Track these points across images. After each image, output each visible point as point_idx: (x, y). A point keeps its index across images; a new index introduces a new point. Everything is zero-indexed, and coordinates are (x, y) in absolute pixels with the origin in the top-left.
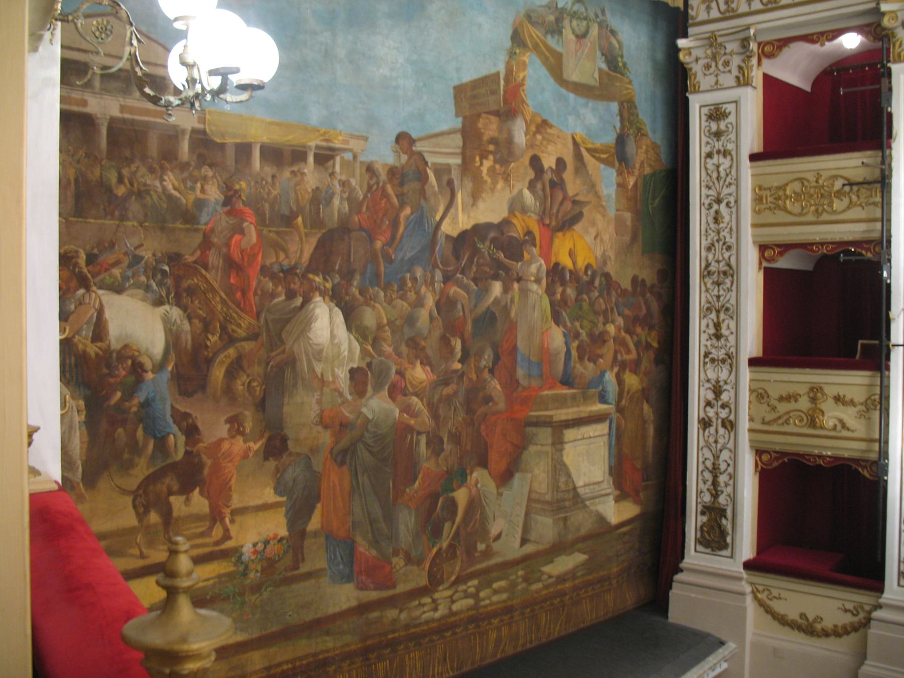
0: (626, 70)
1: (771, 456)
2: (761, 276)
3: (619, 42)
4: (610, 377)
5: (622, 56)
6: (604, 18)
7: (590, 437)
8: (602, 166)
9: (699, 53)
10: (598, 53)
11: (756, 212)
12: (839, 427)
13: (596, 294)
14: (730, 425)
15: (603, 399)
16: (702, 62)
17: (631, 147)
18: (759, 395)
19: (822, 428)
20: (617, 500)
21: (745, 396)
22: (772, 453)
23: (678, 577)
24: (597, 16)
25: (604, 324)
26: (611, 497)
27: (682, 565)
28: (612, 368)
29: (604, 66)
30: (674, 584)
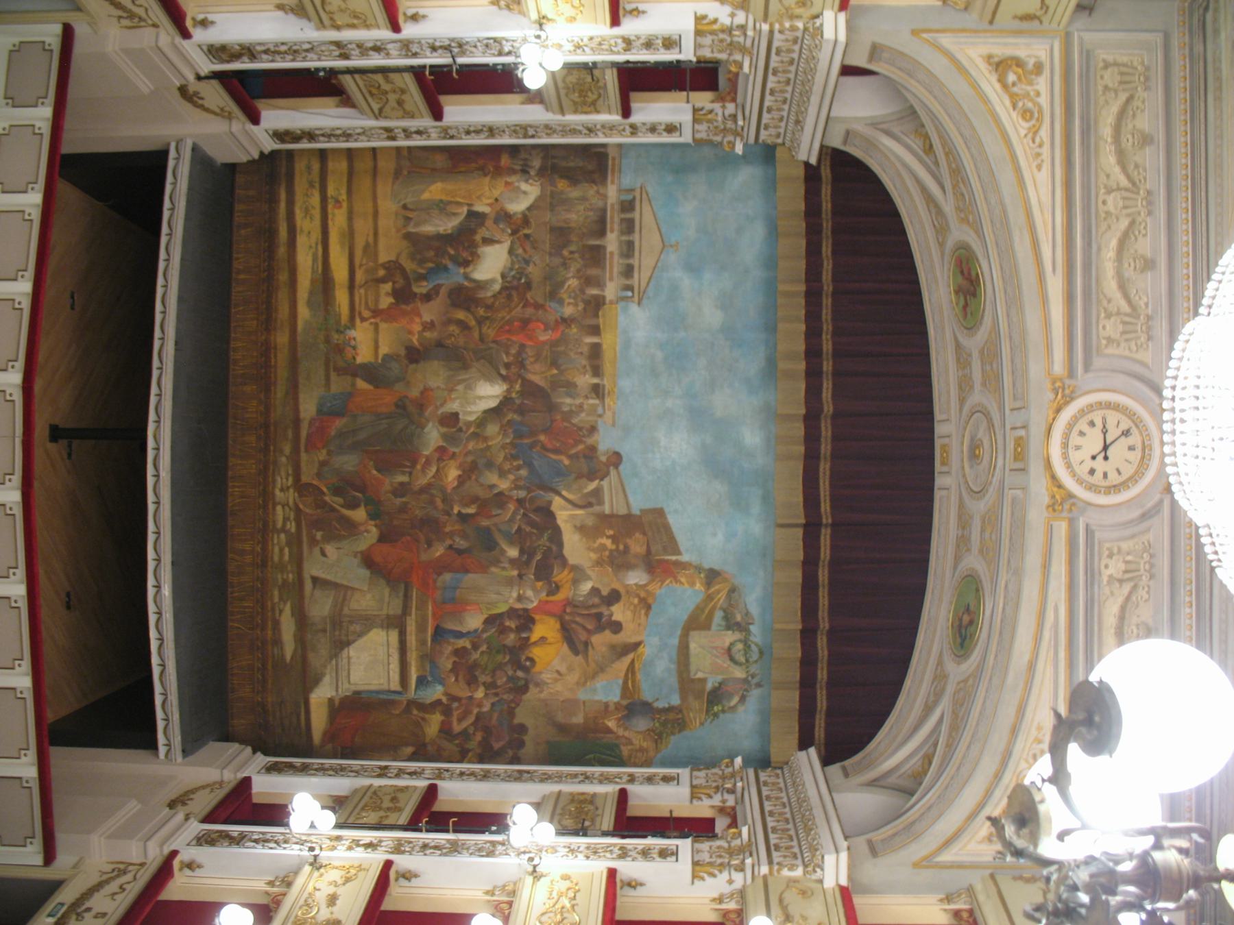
4: (436, 692)
5: (723, 711)
7: (389, 664)
8: (621, 682)
10: (719, 678)
11: (571, 794)
13: (510, 673)
15: (421, 681)
16: (720, 773)
17: (642, 724)
20: (331, 700)
23: (249, 749)
24: (753, 676)
25: (484, 684)
26: (334, 693)
29: (709, 686)
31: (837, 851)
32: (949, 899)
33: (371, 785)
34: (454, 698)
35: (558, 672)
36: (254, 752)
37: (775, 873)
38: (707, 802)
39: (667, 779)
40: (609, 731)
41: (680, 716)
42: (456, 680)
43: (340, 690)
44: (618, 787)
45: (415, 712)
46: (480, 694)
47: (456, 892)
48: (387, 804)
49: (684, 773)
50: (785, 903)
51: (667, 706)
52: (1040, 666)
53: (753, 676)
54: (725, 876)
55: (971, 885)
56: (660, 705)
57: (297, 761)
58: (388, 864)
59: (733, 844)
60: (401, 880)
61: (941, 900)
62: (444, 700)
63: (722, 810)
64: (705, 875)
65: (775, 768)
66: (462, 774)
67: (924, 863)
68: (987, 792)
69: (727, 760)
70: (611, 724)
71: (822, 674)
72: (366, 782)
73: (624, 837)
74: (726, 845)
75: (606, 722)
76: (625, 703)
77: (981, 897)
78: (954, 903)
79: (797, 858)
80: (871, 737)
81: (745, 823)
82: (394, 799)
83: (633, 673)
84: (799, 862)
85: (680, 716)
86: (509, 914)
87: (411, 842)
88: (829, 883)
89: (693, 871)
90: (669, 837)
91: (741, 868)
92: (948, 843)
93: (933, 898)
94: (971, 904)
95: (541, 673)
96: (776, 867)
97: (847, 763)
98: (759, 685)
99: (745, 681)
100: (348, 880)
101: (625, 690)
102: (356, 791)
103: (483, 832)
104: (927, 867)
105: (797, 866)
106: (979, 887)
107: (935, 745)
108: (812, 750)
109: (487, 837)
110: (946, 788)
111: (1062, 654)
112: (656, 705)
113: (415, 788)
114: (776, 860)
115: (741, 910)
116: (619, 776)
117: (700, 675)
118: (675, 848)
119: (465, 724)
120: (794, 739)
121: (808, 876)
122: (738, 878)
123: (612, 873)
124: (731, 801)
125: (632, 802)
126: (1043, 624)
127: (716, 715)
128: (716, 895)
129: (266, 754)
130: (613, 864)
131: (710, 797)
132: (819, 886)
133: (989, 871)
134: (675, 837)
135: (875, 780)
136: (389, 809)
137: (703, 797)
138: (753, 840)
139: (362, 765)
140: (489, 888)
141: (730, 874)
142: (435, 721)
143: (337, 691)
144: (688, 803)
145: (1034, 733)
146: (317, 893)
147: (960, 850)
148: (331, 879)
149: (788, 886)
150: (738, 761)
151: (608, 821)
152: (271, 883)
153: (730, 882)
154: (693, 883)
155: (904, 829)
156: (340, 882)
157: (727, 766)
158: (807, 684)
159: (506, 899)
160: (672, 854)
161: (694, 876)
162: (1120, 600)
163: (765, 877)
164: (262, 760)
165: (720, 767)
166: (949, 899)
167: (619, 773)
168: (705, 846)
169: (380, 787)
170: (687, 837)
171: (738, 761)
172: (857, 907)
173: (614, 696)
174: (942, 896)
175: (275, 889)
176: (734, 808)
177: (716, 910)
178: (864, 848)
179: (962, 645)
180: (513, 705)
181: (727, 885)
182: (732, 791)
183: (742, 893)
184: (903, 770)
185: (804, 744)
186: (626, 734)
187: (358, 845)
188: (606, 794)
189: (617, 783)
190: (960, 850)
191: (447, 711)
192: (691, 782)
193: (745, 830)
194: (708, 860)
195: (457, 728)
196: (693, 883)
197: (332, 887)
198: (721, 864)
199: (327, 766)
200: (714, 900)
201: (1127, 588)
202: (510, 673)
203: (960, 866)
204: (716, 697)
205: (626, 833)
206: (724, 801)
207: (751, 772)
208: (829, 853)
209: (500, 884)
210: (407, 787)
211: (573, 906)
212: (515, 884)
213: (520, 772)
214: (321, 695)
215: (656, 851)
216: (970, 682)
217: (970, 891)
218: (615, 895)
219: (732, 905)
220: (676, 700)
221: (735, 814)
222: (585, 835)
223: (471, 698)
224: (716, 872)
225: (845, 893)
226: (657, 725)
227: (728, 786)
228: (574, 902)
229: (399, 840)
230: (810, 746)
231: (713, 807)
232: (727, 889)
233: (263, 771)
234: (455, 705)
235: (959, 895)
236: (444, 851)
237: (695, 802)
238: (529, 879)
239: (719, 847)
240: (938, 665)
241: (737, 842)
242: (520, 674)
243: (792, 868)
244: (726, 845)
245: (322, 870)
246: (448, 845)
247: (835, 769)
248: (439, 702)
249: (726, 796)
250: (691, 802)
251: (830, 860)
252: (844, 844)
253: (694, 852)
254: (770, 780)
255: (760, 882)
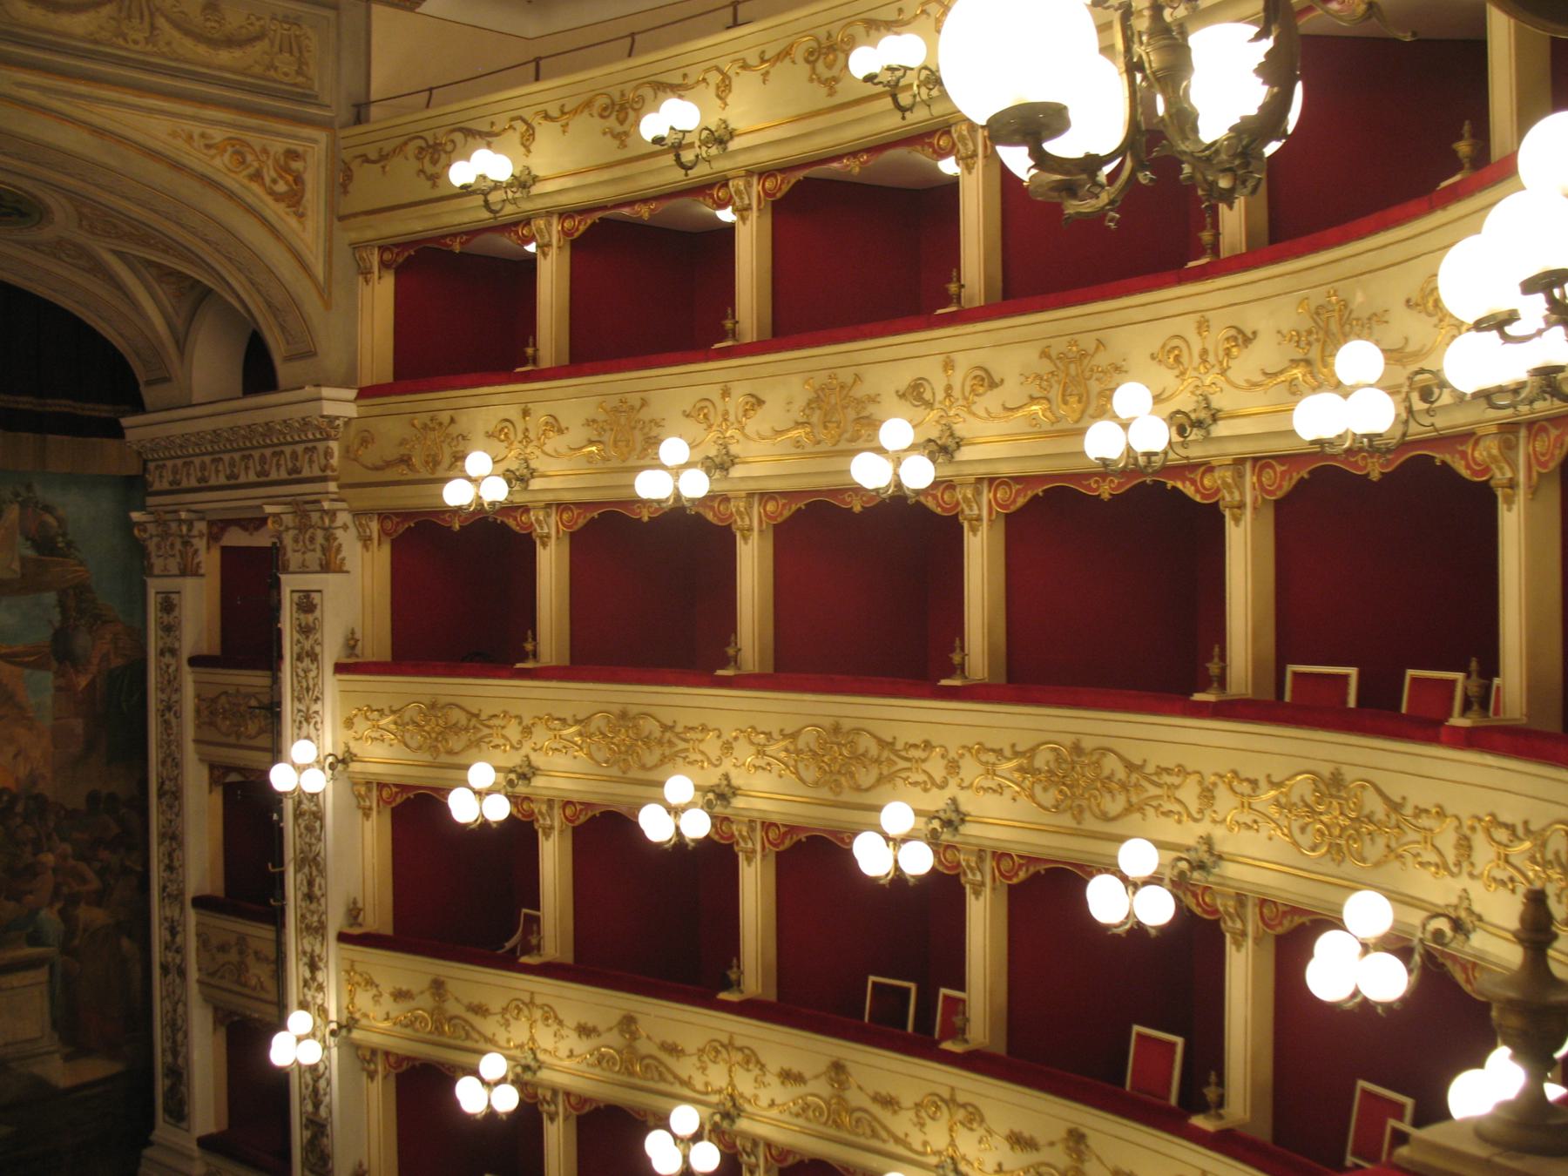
0: (72, 550)
1: (1014, 863)
2: (217, 799)
3: (58, 519)
4: (49, 917)
5: (64, 535)
6: (31, 495)
7: (13, 988)
8: (27, 672)
9: (151, 528)
10: (19, 539)
11: (198, 727)
12: (258, 988)
13: (19, 821)
14: (182, 972)
15: (35, 939)
16: (155, 540)
17: (82, 641)
18: (203, 940)
19: (245, 985)
20: (67, 1058)
21: (192, 944)
22: (1015, 858)
23: (147, 1152)
24: (17, 495)
25: (35, 855)
26: (57, 1056)
27: (153, 1137)
28: (51, 905)
29: (31, 553)
30: (143, 1161)
31: (320, 399)
32: (365, 273)
33: (199, 982)
34: (56, 893)
35: (15, 756)
36: (149, 1144)
37: (335, 473)
38: (203, 556)
39: (168, 606)
40: (91, 684)
41: (71, 592)
42: (31, 892)
43: (52, 1048)
44: (186, 668)
45: (76, 942)
46: (49, 859)
47: (368, 852)
48: (233, 956)
49: (154, 586)
50: (380, 463)
51: (58, 609)
52: (97, 121)
53: (17, 495)
54: (339, 533)
55: (350, 245)
56: (56, 617)
57: (161, 1085)
58: (343, 938)
59: (154, 533)
60: (360, 919)
61: (367, 282)
62: (58, 906)
63: (213, 537)
64: (339, 557)
65: (145, 469)
66: (170, 868)
67: (326, 297)
68: (248, 211)
69: (136, 532)
70: (83, 682)
71: (25, 403)
72: (194, 989)
73: (280, 657)
74: (292, 533)
75: (80, 688)
76: (55, 665)
77: (370, 234)
78: (371, 267)
79: (315, 448)
80: (106, 344)
81: (260, 507)
82: (223, 948)
83: (15, 655)
84: (321, 446)
85: (71, 592)
86: (396, 786)
87: (303, 916)
88: (351, 410)
89: (335, 572)
90: (279, 602)
91: (333, 514)
92: (305, 267)
93: (364, 291)
94: (373, 246)
95: (17, 779)
96: (329, 473)
97: (141, 378)
98: (29, 487)
99: (23, 505)
100: (370, 983)
101: (38, 665)
102: (207, 999)
103: (281, 830)
104: (330, 293)
105: (328, 447)
106: (353, 236)
107: (149, 264)
108: (125, 422)
109: (289, 824)
110: (230, 260)
111: (82, 88)
112: (57, 625)
113: (198, 924)
114: (317, 472)
115: (379, 515)
116: (163, 670)
117: (16, 566)
118: (296, 596)
119: (90, 875)
120: (110, 445)
121: (340, 435)
122: (343, 517)
123: (340, 668)
124: (201, 526)
125: (205, 650)
126: (42, 107)
127: (69, 545)
128: (359, 545)
129: (150, 1125)
130: (328, 668)
131: (196, 551)
132: (354, 422)
133: (335, 221)
134: (279, 593)
135: (177, 342)
136: (241, 952)
137: (196, 561)
138: (289, 499)
139: (162, 999)
140: (360, 813)
141: (195, 537)
142: (91, 916)
143: (48, 1053)
144: (203, 581)
145: (179, 143)
146: (393, 1015)
147: (311, 252)
148: (371, 1003)
149: (355, 460)
150: (136, 516)
151: (254, 680)
152: (372, 1076)
153: (345, 527)
154: (347, 572)
155: (275, 317)
156: (374, 991)
157: (145, 530)
158: (39, 424)
159: (375, 793)
160: (307, 597)
161: (341, 571)
162: (177, 35)
163: (340, 487)
164: (163, 1130)
165: (144, 540)
166: (365, 273)
167: (159, 668)
168: (294, 559)
169: (200, 969)
170: (278, 581)
171: (136, 516)
172: (375, 382)
173: (47, 679)
174: (361, 279)
175: (380, 1068)
176: (211, 523)
177: (379, 544)
178: (298, 367)
179: (22, 214)
180: (63, 812)
181: (348, 531)
182: (190, 523)
183: (357, 514)
184: (170, 310)
185: (117, 432)
186: (95, 661)
187: (314, 978)
188: (195, 682)
189: (177, 669)
190: (311, 252)
191: (73, 900)
192: (175, 576)
193: (269, 509)
194: (319, 554)
195: (95, 884)
196: (347, 572)
197: (382, 1000)
198: (327, 539)
199: (168, 1045)
200: (366, 547)
201: (161, 22)
202: (19, 821)
203: (329, 255)
204: (45, 544)
205: (275, 654)
206: (201, 535)
207: (151, 500)
208: (321, 409)
209: (354, 802)
210: (198, 935)
211: (393, 712)
212: (355, 784)
213: (161, 794)
214: (59, 1073)
215: (302, 616)
216: (86, 210)
217: (356, 247)
218: (375, 664)
219: (375, 526)
220: (50, 597)
221: (221, 521)
222: (279, 704)
223: (55, 870)
224: (336, 544)
225: (365, 393)
226: (83, 622)
227: (184, 529)
228: (387, 712)
229: (299, 931)
230: (118, 423)
231: (208, 548)
232: (353, 531)
233: (184, 1125)
234: (65, 890)
235: (362, 258)
236: (315, 873)
237: (202, 571)
238: (355, 767)
239: (296, 540)
240: (36, 249)
241: (288, 520)
242: (19, 808)
243: (328, 454)
244: (292, 533)
245: (357, 1016)
246: (306, 870)
247: (149, 395)
248: (61, 912)
249: (195, 532)
250: (202, 575)
251: (329, 409)
252: (309, 391)
253: (304, 569)
254: (168, 475)
255: (348, 492)
